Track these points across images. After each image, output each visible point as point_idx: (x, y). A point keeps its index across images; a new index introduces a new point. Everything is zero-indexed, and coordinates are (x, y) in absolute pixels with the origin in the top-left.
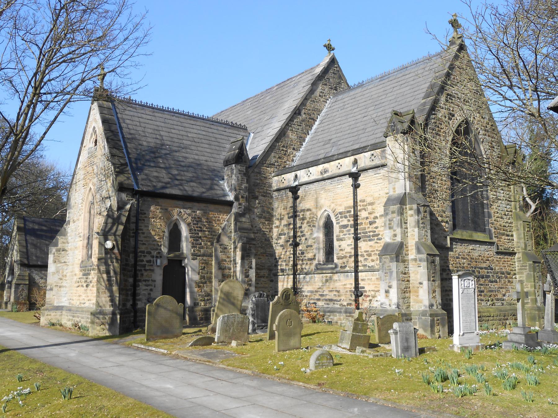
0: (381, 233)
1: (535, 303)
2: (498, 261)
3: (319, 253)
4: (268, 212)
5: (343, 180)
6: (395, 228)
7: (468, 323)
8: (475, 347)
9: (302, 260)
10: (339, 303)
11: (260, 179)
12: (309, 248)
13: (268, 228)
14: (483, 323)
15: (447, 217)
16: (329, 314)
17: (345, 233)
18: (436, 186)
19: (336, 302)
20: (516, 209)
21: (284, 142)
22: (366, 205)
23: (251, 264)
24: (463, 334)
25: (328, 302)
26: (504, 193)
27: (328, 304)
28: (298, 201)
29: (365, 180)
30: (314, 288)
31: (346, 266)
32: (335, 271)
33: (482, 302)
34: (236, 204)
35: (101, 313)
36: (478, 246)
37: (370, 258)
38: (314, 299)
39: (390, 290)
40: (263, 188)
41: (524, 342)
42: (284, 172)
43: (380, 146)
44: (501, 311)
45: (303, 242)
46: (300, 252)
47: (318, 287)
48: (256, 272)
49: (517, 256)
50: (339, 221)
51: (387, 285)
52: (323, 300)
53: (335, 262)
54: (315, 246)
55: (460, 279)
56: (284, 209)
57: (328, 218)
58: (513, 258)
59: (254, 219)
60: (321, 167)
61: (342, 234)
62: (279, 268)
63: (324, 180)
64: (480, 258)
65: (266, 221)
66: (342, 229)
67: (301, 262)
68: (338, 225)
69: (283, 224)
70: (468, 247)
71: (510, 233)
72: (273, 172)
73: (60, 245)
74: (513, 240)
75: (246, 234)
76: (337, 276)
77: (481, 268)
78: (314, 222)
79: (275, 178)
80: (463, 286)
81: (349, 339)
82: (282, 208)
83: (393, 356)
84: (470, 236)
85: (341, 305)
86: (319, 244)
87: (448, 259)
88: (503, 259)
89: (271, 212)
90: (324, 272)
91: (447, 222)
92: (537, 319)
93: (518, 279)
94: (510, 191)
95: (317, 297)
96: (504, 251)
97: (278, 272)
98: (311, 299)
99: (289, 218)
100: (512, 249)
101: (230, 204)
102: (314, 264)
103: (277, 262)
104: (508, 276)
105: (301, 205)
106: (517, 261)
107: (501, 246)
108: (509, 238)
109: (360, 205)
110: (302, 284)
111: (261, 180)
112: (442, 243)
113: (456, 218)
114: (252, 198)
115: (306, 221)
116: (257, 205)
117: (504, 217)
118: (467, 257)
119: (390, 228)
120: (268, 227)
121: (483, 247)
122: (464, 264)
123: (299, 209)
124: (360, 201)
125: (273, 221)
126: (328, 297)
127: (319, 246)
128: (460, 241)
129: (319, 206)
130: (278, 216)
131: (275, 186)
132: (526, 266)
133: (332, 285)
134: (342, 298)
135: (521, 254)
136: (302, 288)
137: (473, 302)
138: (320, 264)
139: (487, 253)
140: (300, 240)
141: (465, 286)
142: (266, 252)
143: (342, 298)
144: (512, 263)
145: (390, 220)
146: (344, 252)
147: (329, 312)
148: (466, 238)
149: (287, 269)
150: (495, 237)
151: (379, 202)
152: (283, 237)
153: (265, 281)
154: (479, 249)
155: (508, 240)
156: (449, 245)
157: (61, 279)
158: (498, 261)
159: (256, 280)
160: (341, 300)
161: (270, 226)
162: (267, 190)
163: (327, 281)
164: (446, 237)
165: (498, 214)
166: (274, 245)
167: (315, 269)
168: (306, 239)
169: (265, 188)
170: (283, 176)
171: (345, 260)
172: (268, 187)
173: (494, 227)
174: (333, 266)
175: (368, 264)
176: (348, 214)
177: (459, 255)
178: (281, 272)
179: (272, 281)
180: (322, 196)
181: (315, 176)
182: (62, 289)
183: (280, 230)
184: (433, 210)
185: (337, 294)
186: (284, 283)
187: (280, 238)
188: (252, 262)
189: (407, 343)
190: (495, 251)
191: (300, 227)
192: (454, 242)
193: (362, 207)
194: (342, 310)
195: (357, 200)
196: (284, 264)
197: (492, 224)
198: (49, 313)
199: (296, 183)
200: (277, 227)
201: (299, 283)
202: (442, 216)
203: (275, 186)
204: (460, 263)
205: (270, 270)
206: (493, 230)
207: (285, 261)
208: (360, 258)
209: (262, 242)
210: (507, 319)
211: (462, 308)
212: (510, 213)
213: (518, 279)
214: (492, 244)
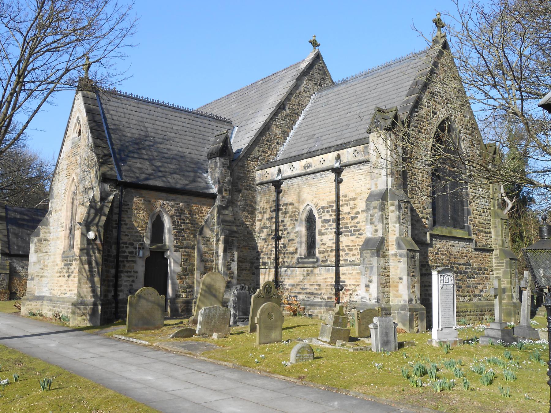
0: (362, 228)
3: (301, 247)
4: (251, 206)
5: (326, 175)
6: (376, 223)
8: (453, 342)
9: (284, 254)
10: (319, 296)
13: (251, 222)
15: (427, 213)
16: (309, 307)
19: (316, 296)
21: (268, 136)
22: (348, 201)
23: (234, 257)
24: (442, 329)
25: (309, 296)
26: (483, 191)
27: (309, 298)
28: (281, 195)
29: (348, 176)
31: (327, 260)
32: (316, 265)
33: (460, 297)
34: (219, 197)
35: (83, 303)
36: (457, 242)
37: (352, 253)
39: (370, 284)
40: (247, 182)
42: (268, 166)
43: (363, 142)
44: (478, 306)
47: (299, 280)
48: (238, 265)
49: (494, 253)
51: (368, 279)
52: (303, 293)
54: (297, 240)
55: (439, 275)
56: (267, 203)
57: (311, 211)
58: (490, 254)
59: (237, 212)
60: (304, 162)
61: (324, 228)
62: (261, 261)
63: (307, 174)
64: (459, 254)
65: (249, 214)
67: (282, 256)
68: (320, 220)
69: (265, 218)
70: (447, 243)
71: (488, 230)
72: (257, 166)
73: (42, 235)
74: (491, 237)
76: (318, 270)
77: (460, 264)
78: (297, 216)
80: (442, 281)
81: (329, 333)
82: (265, 202)
85: (322, 298)
86: (301, 237)
87: (427, 255)
88: (481, 256)
89: (254, 205)
90: (306, 265)
91: (427, 218)
93: (495, 275)
95: (298, 290)
97: (260, 265)
98: (292, 292)
100: (489, 246)
101: (213, 197)
103: (259, 255)
104: (486, 272)
105: (284, 199)
106: (495, 258)
107: (479, 242)
108: (487, 235)
111: (245, 174)
115: (288, 215)
116: (240, 198)
117: (483, 214)
118: (446, 253)
119: (371, 223)
122: (443, 260)
123: (281, 203)
124: (342, 196)
126: (309, 291)
127: (301, 240)
132: (503, 263)
133: (313, 279)
134: (323, 292)
135: (498, 251)
136: (283, 281)
137: (452, 297)
138: (302, 258)
139: (465, 249)
140: (282, 234)
141: (445, 281)
143: (323, 292)
144: (489, 260)
145: (371, 216)
146: (325, 247)
147: (310, 305)
149: (269, 262)
150: (474, 234)
151: (361, 197)
152: (265, 230)
153: (247, 274)
156: (429, 241)
157: (42, 269)
160: (321, 293)
162: (250, 183)
163: (308, 274)
164: (426, 233)
165: (477, 212)
166: (256, 239)
167: (296, 263)
168: (288, 233)
170: (266, 170)
171: (326, 254)
173: (473, 224)
174: (315, 260)
175: (349, 259)
176: (330, 209)
177: (438, 251)
178: (263, 265)
179: (254, 274)
182: (43, 279)
183: (262, 224)
185: (317, 287)
186: (265, 276)
187: (263, 232)
188: (234, 255)
189: (387, 338)
190: (473, 248)
191: (283, 221)
194: (323, 304)
197: (471, 221)
198: (29, 303)
200: (260, 220)
201: (280, 276)
202: (422, 213)
204: (439, 259)
205: (252, 263)
206: (472, 227)
208: (341, 253)
209: (244, 235)
210: (484, 315)
211: (441, 303)
213: (495, 275)
214: (470, 240)
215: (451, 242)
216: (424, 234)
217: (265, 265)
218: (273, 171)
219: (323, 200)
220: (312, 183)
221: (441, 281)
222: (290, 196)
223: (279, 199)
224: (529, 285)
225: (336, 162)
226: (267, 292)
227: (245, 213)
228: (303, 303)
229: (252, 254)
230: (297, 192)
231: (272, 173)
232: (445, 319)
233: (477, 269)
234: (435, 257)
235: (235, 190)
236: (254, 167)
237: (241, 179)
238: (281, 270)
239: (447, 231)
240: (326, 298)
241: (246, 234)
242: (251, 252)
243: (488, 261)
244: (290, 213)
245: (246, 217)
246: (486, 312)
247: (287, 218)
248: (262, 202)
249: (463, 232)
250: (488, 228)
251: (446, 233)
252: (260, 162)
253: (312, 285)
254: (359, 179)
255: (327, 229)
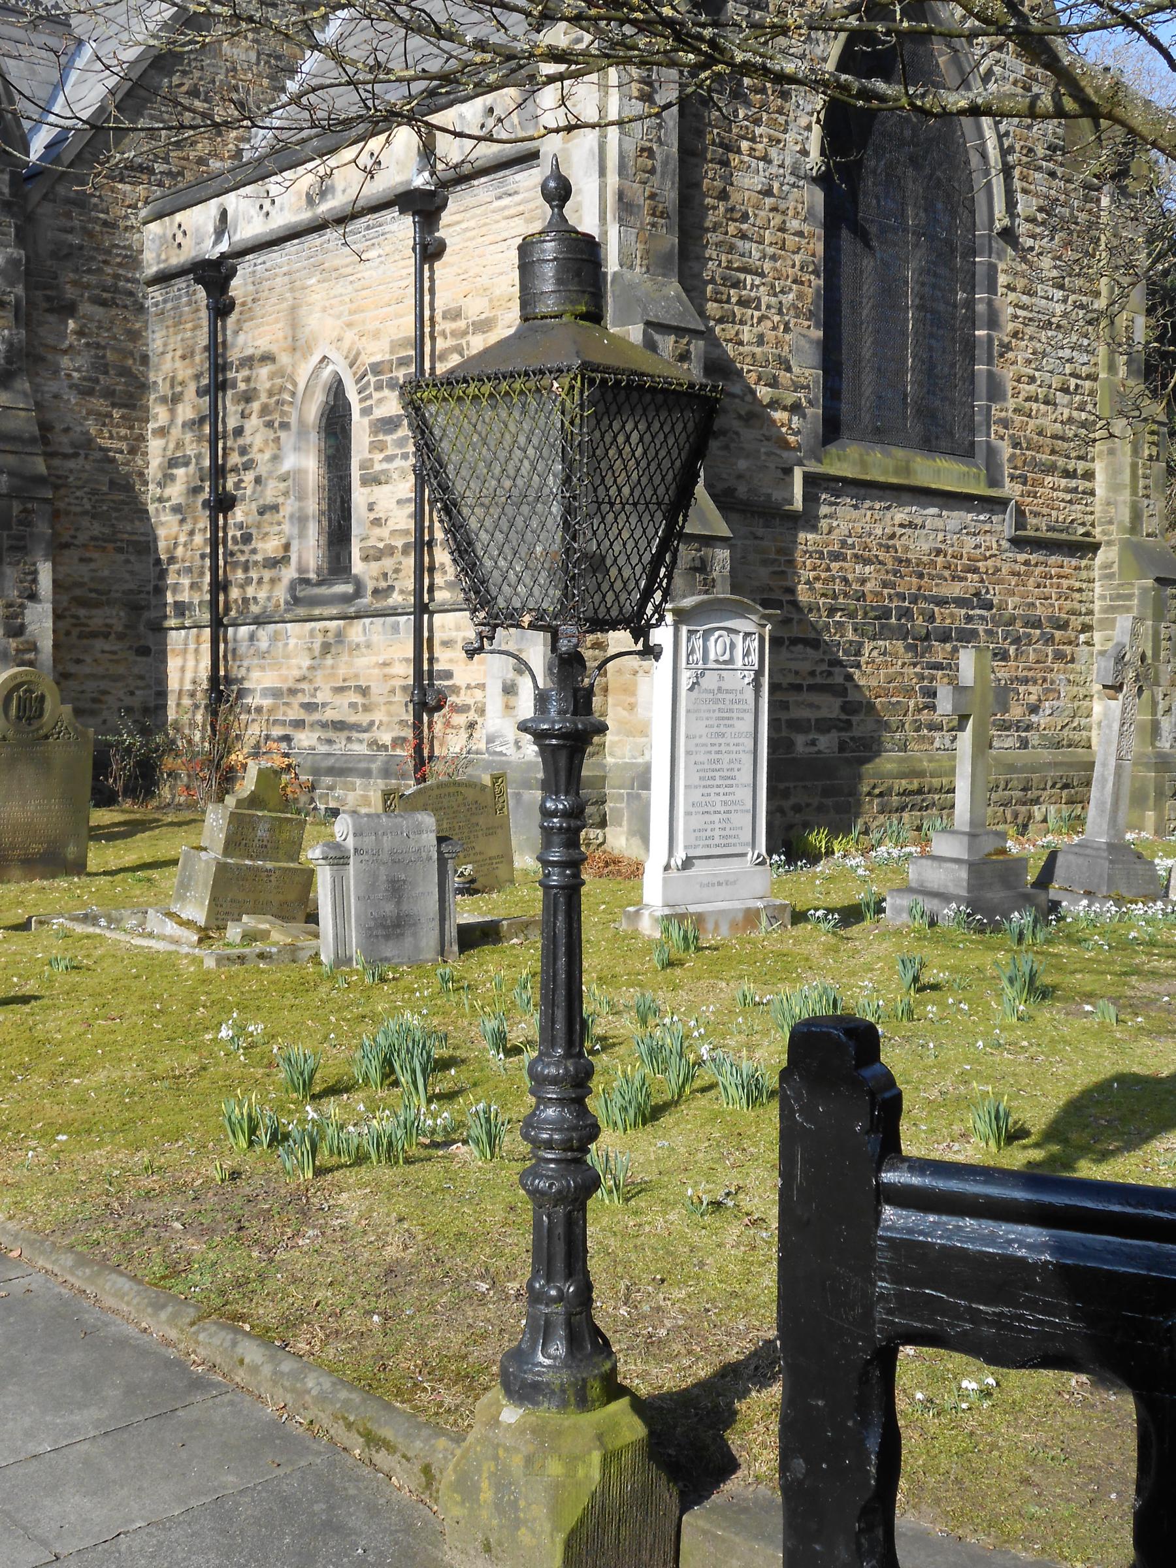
1: (1148, 739)
2: (1019, 574)
3: (302, 535)
4: (125, 372)
5: (386, 228)
7: (716, 817)
8: (740, 916)
9: (246, 569)
10: (365, 736)
11: (84, 229)
12: (267, 516)
13: (125, 438)
14: (930, 816)
15: (797, 387)
16: (328, 780)
17: (389, 452)
18: (756, 254)
19: (355, 735)
20: (1112, 368)
21: (197, 74)
22: (465, 333)
23: (35, 581)
24: (687, 863)
25: (330, 734)
26: (1065, 301)
27: (330, 742)
28: (232, 320)
29: (464, 225)
30: (285, 680)
31: (391, 588)
32: (352, 610)
33: (937, 734)
36: (933, 511)
38: (283, 723)
40: (99, 271)
41: (964, 893)
42: (183, 200)
44: (1012, 768)
45: (248, 492)
46: (238, 534)
47: (297, 673)
48: (57, 616)
50: (368, 403)
52: (312, 725)
53: (355, 571)
54: (289, 507)
55: (684, 629)
56: (183, 357)
57: (337, 389)
58: (1084, 563)
59: (56, 396)
61: (381, 456)
62: (170, 599)
63: (318, 227)
64: (940, 559)
65: (114, 405)
66: (381, 437)
67: (240, 575)
68: (366, 421)
69: (179, 421)
70: (889, 515)
71: (1081, 466)
72: (146, 203)
74: (1092, 493)
75: (11, 460)
76: (360, 628)
77: (942, 602)
78: (286, 408)
79: (153, 226)
80: (698, 655)
81: (205, 884)
82: (179, 353)
83: (323, 958)
84: (897, 472)
85: (373, 743)
86: (301, 498)
87: (791, 562)
88: (1040, 569)
89: (137, 368)
90: (317, 612)
91: (795, 408)
92: (1151, 802)
93: (1098, 648)
94: (1097, 294)
95: (295, 713)
96: (1055, 535)
97: (165, 617)
98: (275, 722)
99: (200, 393)
100: (1081, 530)
102: (285, 582)
103: (163, 574)
104: (1058, 634)
105: (241, 338)
107: (1036, 514)
108: (1073, 483)
109: (443, 334)
110: (245, 664)
111: (90, 234)
112: (769, 496)
113: (846, 395)
114: (47, 311)
115: (256, 406)
116: (71, 339)
117: (1061, 398)
118: (882, 555)
120: (123, 432)
121: (956, 518)
122: (863, 582)
123: (234, 355)
125: (147, 409)
126: (329, 715)
127: (301, 509)
128: (854, 491)
129: (301, 342)
130: (164, 389)
131: (151, 264)
132: (1129, 597)
133: (344, 666)
134: (378, 716)
135: (1116, 548)
136: (243, 679)
137: (747, 725)
138: (306, 582)
139: (970, 542)
140: (237, 486)
141: (712, 656)
142: (114, 533)
143: (378, 716)
144: (1077, 585)
146: (384, 532)
147: (332, 771)
148: (881, 479)
149: (196, 601)
150: (1012, 478)
152: (180, 472)
153: (114, 653)
154: (939, 523)
155: (1068, 490)
156: (798, 504)
158: (1019, 574)
159: (56, 646)
160: (372, 723)
161: (131, 428)
162: (117, 277)
163: (326, 648)
164: (789, 471)
165: (1032, 388)
166: (151, 508)
167: (287, 603)
168: (258, 480)
169: (109, 270)
170: (179, 217)
172: (120, 265)
173: (1012, 437)
174: (349, 589)
177: (843, 543)
178: (176, 616)
179: (144, 651)
180: (315, 297)
181: (286, 212)
183: (172, 446)
184: (731, 354)
185: (357, 699)
186: (185, 660)
187: (172, 478)
188: (35, 573)
189: (398, 903)
190: (1007, 535)
191: (239, 432)
192: (826, 490)
193: (451, 342)
194: (374, 766)
195: (432, 309)
196: (186, 581)
197: (1005, 423)
199: (224, 247)
200: (162, 432)
201: (234, 660)
202: (774, 383)
203: (151, 264)
204: (845, 580)
205: (136, 608)
206: (1006, 450)
207: (189, 570)
209: (94, 492)
210: (1036, 801)
211: (688, 753)
212: (1088, 384)
213: (1098, 648)
214: (1002, 503)
215: (907, 509)
216: (780, 474)
217: (183, 615)
218: (201, 222)
219: (376, 335)
220: (338, 262)
221: (691, 653)
222: (262, 324)
223: (224, 342)
224: (1131, 675)
225: (420, 171)
226: (19, 718)
227: (99, 404)
228: (309, 764)
229: (132, 573)
230: (285, 305)
231: (197, 230)
232: (707, 818)
233: (1019, 624)
234: (828, 569)
235: (45, 305)
236: (135, 207)
237: (68, 256)
238: (235, 633)
239: (890, 463)
240: (389, 743)
241: (105, 489)
242: (128, 561)
243: (1070, 588)
244: (263, 398)
245: (103, 418)
246: (1048, 792)
247: (254, 416)
248: (169, 356)
249: (964, 469)
250: (1079, 458)
251: (885, 472)
252: (160, 184)
253: (339, 690)
254: (505, 235)
255: (389, 459)
